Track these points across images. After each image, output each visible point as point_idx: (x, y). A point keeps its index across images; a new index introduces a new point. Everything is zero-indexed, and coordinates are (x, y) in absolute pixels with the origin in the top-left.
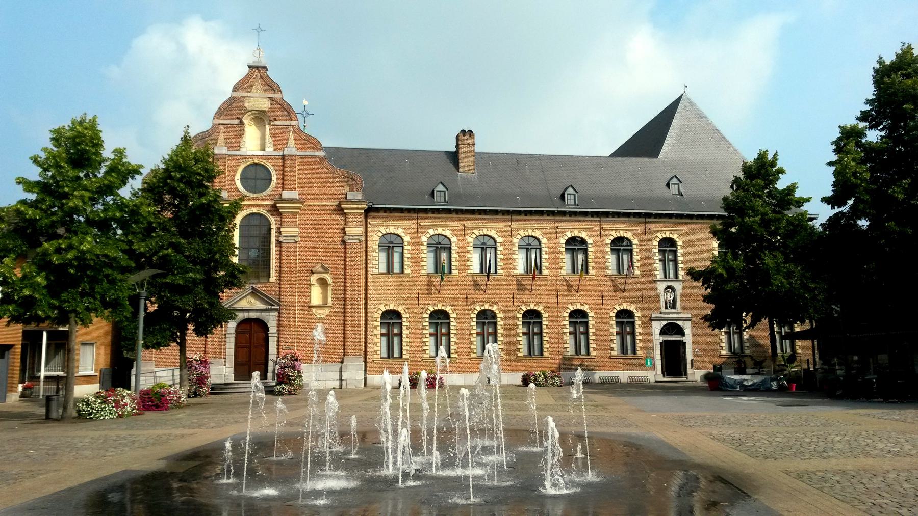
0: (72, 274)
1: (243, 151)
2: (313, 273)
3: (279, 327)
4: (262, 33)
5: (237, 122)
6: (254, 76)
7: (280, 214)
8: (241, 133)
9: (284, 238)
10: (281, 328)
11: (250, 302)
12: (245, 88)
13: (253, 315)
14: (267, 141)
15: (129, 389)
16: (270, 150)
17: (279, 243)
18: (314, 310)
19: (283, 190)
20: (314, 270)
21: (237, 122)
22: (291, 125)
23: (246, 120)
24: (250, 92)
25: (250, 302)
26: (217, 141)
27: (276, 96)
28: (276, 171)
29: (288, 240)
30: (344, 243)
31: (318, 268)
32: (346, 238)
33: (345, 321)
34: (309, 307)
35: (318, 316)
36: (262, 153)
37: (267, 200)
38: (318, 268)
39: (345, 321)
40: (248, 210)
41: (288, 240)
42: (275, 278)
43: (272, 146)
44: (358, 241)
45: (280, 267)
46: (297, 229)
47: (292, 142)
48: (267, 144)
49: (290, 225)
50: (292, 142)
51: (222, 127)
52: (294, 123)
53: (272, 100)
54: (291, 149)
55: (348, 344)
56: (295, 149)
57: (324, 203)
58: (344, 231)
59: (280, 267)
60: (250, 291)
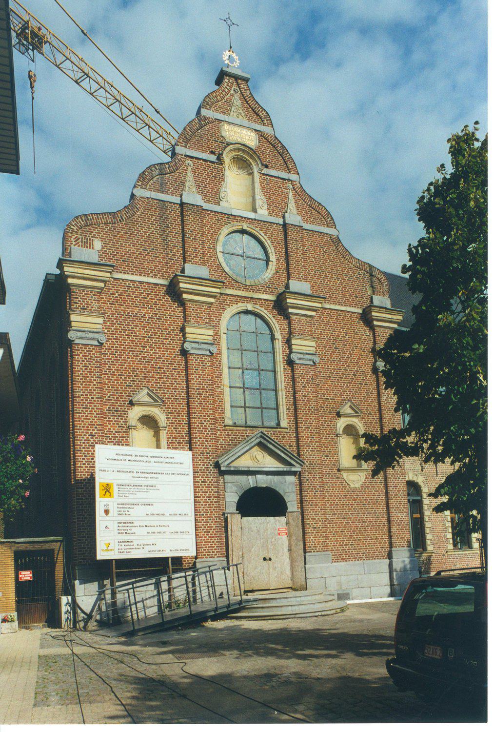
0: (411, 418)
1: (224, 207)
2: (339, 415)
3: (301, 501)
4: (233, 28)
5: (213, 158)
6: (232, 92)
7: (287, 316)
8: (220, 178)
9: (79, 334)
10: (305, 503)
11: (254, 458)
12: (220, 107)
13: (263, 481)
14: (257, 197)
15: (60, 627)
16: (263, 213)
17: (290, 363)
18: (345, 475)
19: (185, 262)
20: (135, 400)
21: (213, 158)
22: (289, 180)
23: (227, 158)
24: (228, 114)
25: (254, 458)
26: (183, 183)
27: (267, 130)
28: (275, 248)
29: (303, 359)
30: (184, 353)
31: (347, 409)
32: (187, 346)
33: (387, 493)
34: (339, 470)
35: (352, 486)
36: (252, 215)
37: (266, 292)
38: (347, 409)
39: (387, 493)
40: (240, 304)
41: (303, 359)
42: (287, 421)
43: (266, 206)
44: (96, 343)
45: (295, 404)
46: (101, 321)
47: (292, 206)
48: (259, 203)
49: (303, 335)
50: (292, 206)
51: (189, 162)
52: (293, 177)
53: (261, 135)
54: (293, 217)
55: (394, 530)
56: (266, 213)
57: (343, 308)
58: (183, 330)
59: (295, 404)
60: (258, 440)
